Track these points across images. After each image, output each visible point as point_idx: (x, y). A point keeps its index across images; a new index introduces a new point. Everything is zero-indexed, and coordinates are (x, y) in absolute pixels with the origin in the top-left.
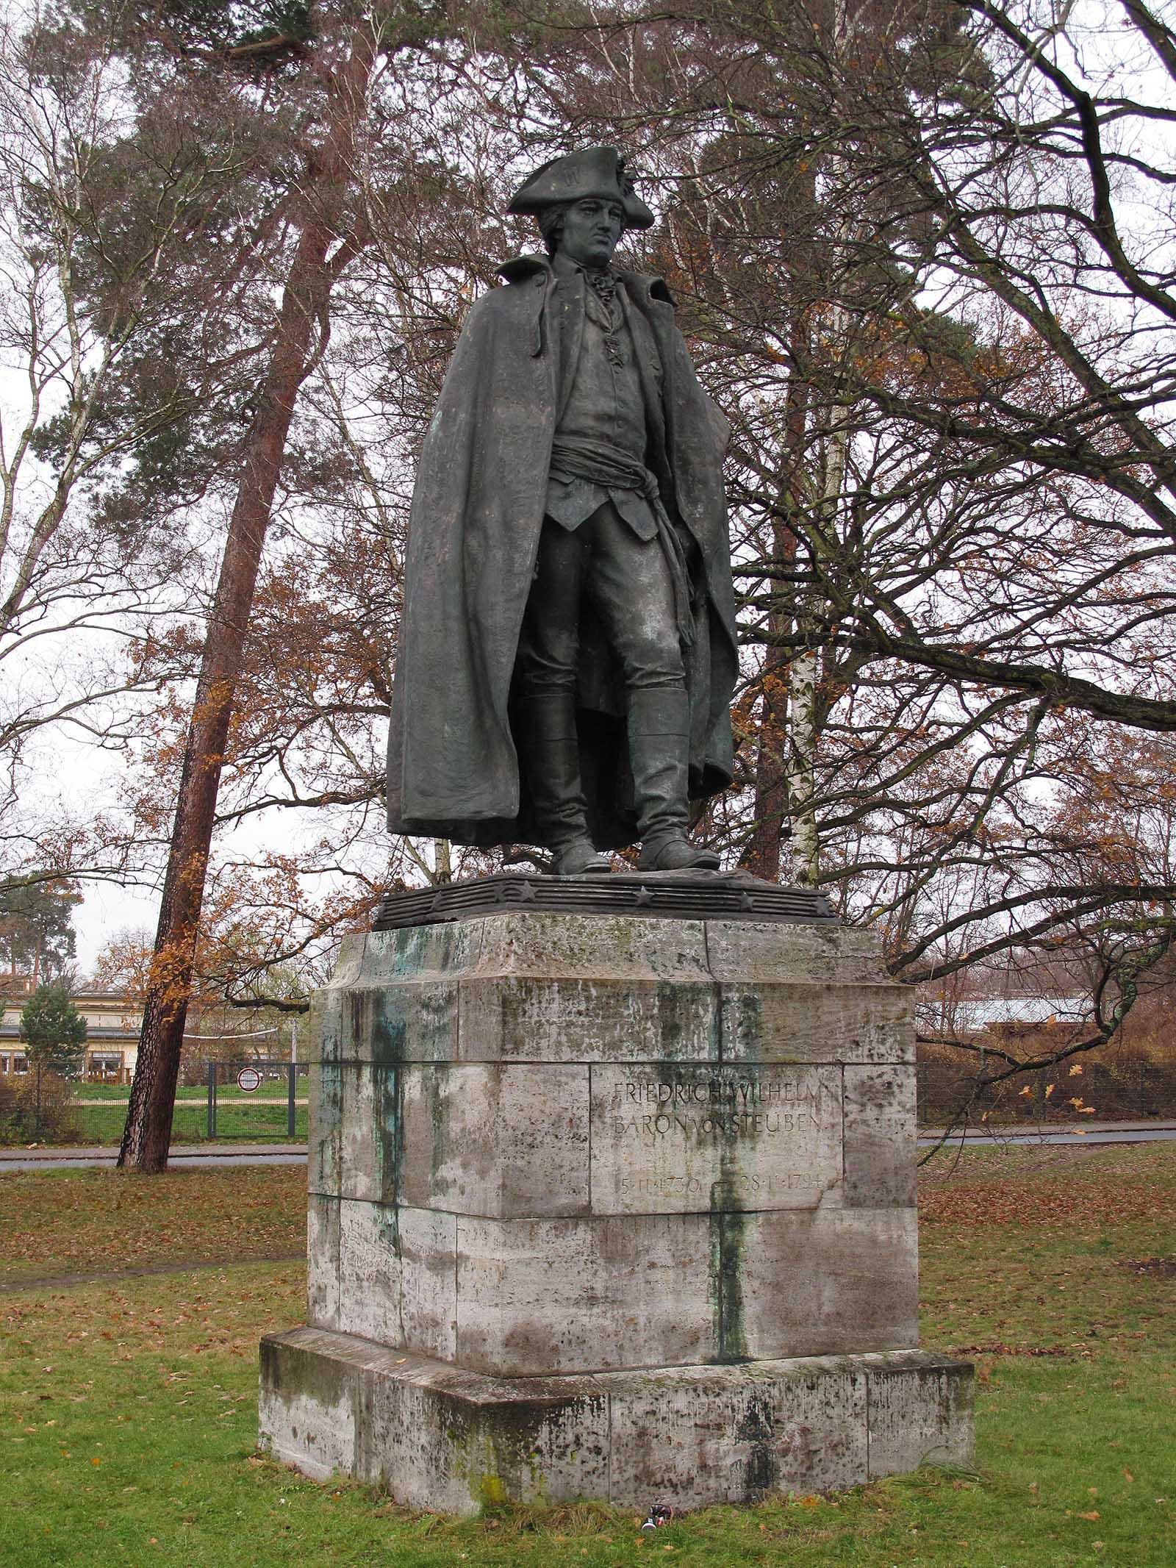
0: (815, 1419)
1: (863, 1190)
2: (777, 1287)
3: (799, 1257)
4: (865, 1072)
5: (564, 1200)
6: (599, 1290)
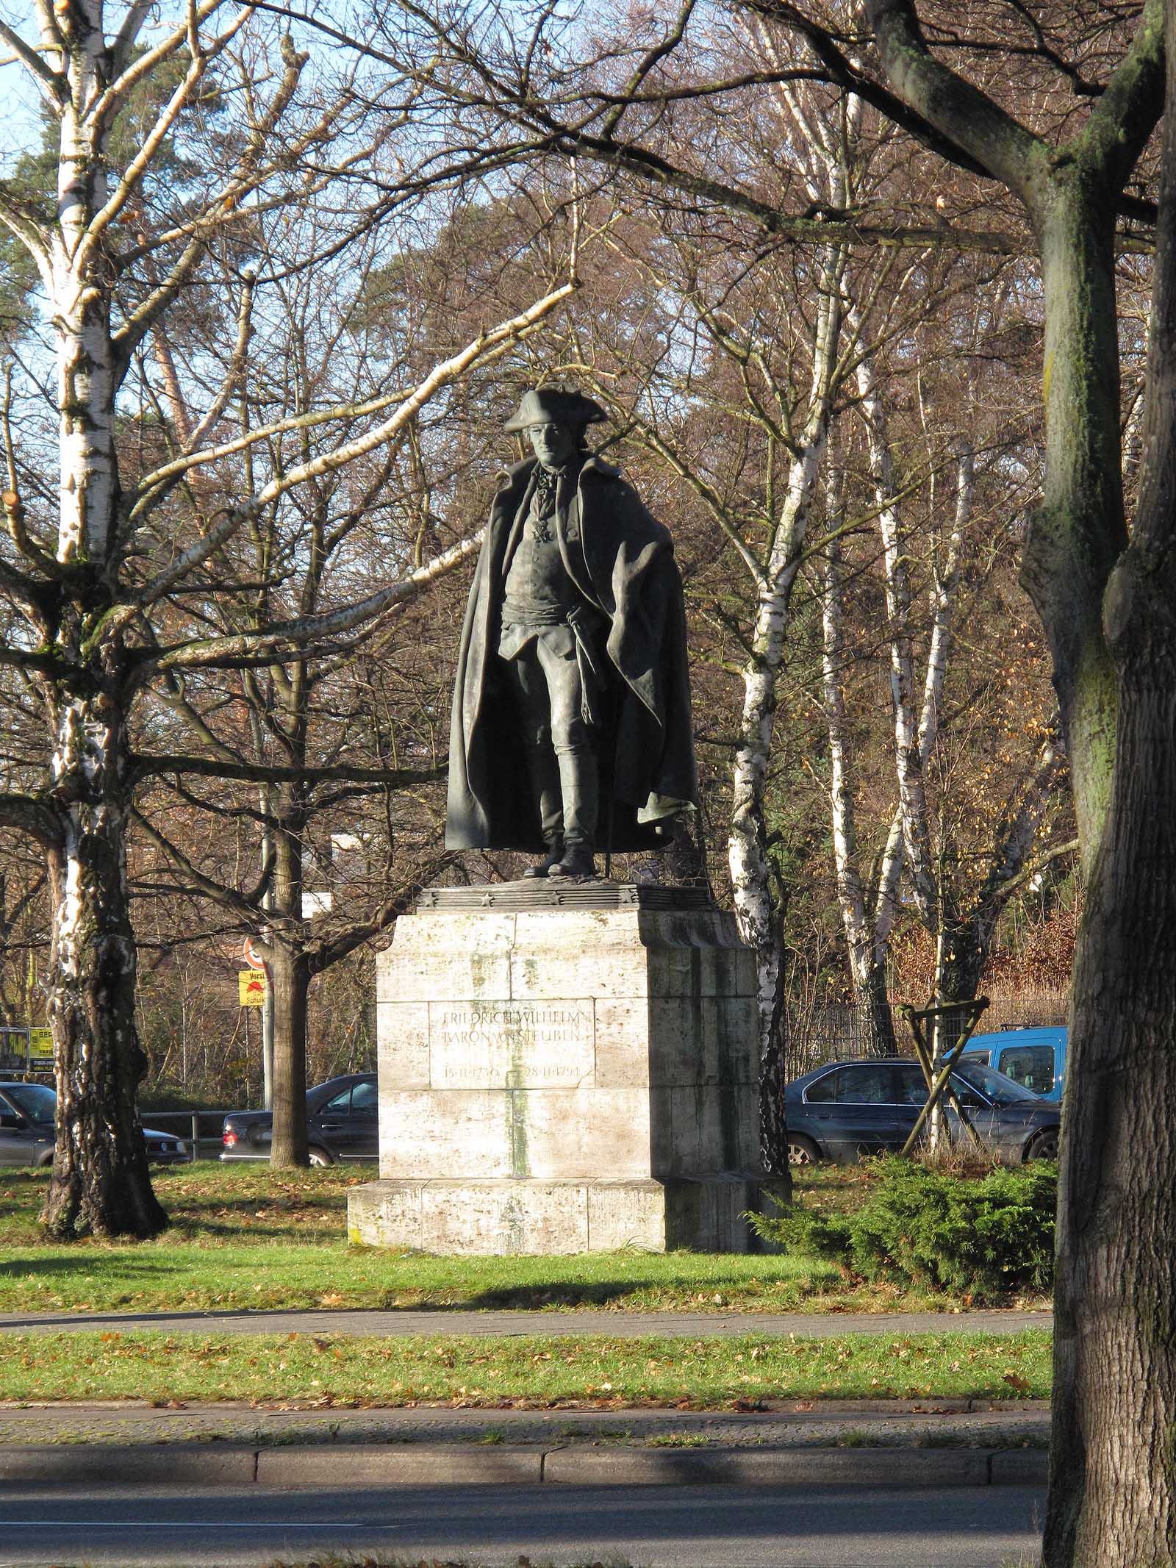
0: (552, 1213)
1: (609, 1077)
2: (551, 1134)
3: (564, 1118)
4: (609, 1004)
5: (415, 1080)
6: (437, 1133)
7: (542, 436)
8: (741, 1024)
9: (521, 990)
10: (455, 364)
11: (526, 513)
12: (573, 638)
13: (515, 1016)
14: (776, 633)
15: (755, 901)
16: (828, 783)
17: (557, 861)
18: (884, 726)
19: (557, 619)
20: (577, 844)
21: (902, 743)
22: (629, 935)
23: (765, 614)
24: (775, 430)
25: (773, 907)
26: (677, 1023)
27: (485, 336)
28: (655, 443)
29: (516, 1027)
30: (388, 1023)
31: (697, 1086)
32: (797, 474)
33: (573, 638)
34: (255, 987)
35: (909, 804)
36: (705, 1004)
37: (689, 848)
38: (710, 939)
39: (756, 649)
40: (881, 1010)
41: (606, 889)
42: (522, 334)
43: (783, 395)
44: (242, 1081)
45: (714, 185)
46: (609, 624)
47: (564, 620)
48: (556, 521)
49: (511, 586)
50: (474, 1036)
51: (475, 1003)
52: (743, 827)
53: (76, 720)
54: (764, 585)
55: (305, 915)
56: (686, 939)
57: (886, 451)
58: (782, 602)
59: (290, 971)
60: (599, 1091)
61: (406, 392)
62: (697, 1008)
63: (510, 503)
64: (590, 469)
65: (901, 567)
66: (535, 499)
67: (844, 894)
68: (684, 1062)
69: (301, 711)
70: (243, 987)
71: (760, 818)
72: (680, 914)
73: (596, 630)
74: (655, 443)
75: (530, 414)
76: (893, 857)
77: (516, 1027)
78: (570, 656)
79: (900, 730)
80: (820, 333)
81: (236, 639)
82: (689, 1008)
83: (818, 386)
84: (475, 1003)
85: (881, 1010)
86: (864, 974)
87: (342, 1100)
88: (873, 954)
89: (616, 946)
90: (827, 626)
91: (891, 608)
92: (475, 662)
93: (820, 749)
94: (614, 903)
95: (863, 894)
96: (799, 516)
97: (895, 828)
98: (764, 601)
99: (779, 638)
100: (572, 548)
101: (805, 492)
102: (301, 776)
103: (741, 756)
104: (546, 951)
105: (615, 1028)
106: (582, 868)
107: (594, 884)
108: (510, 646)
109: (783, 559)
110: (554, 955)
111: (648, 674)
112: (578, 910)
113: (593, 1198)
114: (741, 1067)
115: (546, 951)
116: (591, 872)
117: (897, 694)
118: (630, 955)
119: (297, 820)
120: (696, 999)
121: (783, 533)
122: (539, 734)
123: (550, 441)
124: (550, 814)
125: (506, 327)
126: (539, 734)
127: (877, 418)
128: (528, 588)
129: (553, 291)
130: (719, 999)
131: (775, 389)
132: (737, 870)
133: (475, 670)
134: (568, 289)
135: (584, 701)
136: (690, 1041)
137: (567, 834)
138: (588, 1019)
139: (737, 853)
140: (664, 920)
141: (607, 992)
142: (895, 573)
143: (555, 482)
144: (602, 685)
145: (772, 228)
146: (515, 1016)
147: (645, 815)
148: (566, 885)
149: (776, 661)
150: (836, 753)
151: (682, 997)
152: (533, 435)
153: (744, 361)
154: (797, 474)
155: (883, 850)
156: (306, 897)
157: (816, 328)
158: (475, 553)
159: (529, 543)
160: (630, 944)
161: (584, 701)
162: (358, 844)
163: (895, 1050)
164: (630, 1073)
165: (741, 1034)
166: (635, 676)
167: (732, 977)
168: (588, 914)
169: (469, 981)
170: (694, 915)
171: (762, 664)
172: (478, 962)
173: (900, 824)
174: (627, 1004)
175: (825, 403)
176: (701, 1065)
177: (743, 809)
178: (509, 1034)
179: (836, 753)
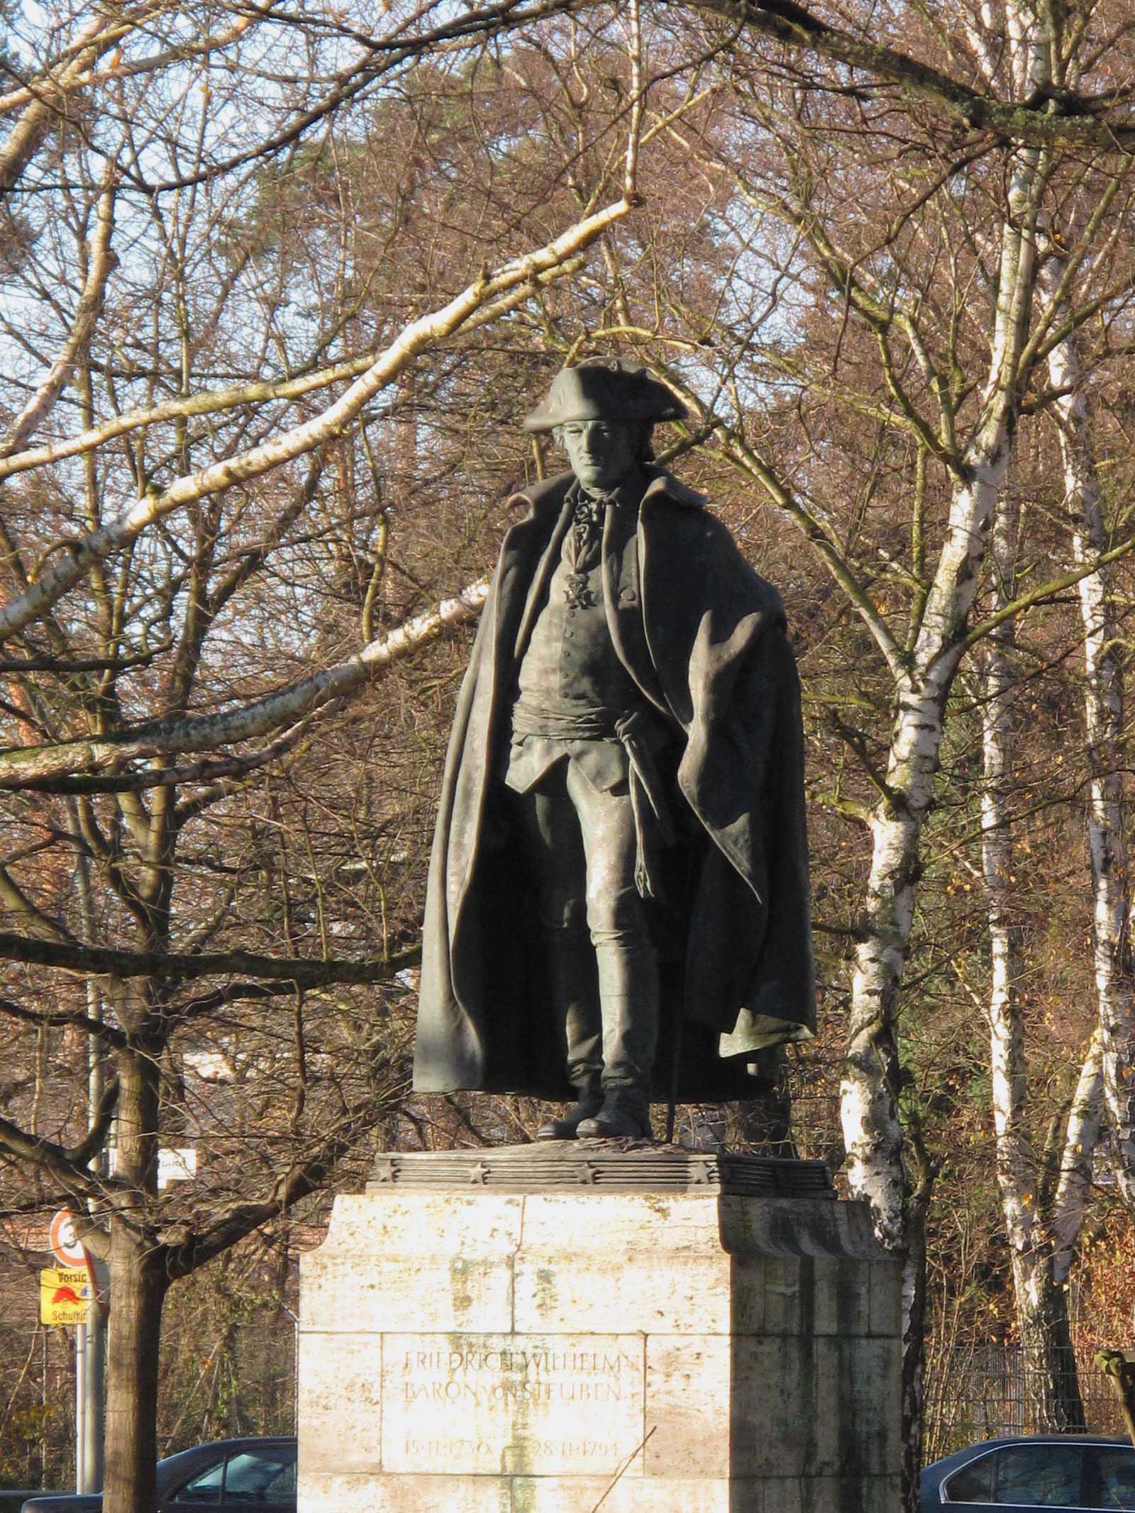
1: (666, 1460)
4: (669, 1343)
5: (356, 1457)
7: (583, 441)
8: (877, 1381)
9: (528, 1318)
10: (438, 322)
11: (555, 561)
12: (624, 760)
13: (518, 1359)
14: (924, 757)
15: (881, 1181)
16: (985, 993)
17: (590, 1114)
18: (1073, 905)
19: (601, 730)
20: (623, 1089)
21: (1102, 935)
22: (702, 1236)
23: (907, 726)
24: (931, 437)
25: (908, 1191)
26: (775, 1378)
27: (488, 278)
28: (739, 452)
29: (519, 1375)
30: (318, 1366)
31: (804, 1476)
32: (962, 506)
33: (624, 760)
34: (65, 1294)
35: (1113, 1031)
36: (820, 1347)
37: (756, 1092)
38: (830, 1243)
39: (892, 782)
40: (1060, 1356)
41: (669, 1160)
42: (543, 277)
43: (944, 382)
44: (33, 1442)
45: (887, 53)
46: (681, 741)
47: (612, 733)
48: (602, 575)
49: (529, 676)
50: (453, 1389)
51: (456, 1337)
52: (865, 1065)
54: (907, 682)
55: (162, 1184)
56: (793, 1243)
57: (1090, 472)
58: (934, 709)
59: (136, 1273)
60: (651, 1482)
61: (359, 363)
62: (807, 1354)
63: (529, 546)
64: (658, 495)
65: (1112, 656)
66: (569, 539)
67: (1005, 1172)
68: (786, 1439)
69: (165, 862)
70: (46, 1296)
71: (892, 1051)
72: (784, 1203)
73: (662, 749)
74: (739, 452)
75: (565, 403)
76: (1084, 1114)
77: (519, 1375)
78: (619, 789)
79: (1102, 912)
80: (1004, 286)
81: (78, 747)
82: (795, 1354)
83: (999, 367)
84: (456, 1337)
85: (1060, 1356)
86: (1035, 1299)
87: (211, 1479)
88: (1050, 1268)
89: (682, 1253)
90: (990, 749)
91: (1091, 720)
92: (468, 794)
93: (977, 942)
94: (680, 1183)
95: (1037, 1172)
96: (964, 573)
97: (1088, 1068)
98: (907, 707)
99: (928, 766)
100: (627, 619)
101: (973, 536)
102: (160, 967)
103: (864, 951)
104: (570, 1257)
105: (677, 1382)
106: (628, 1124)
107: (649, 1152)
108: (524, 771)
109: (937, 641)
110: (582, 1263)
111: (742, 821)
112: (621, 1192)
114: (874, 1448)
115: (570, 1257)
116: (643, 1133)
117: (1099, 858)
118: (703, 1267)
119: (154, 1034)
120: (806, 1339)
121: (939, 598)
122: (567, 913)
123: (596, 448)
124: (582, 1037)
125: (520, 265)
126: (567, 913)
127: (1078, 421)
128: (556, 680)
129: (594, 211)
130: (844, 1338)
131: (932, 372)
132: (854, 1134)
133: (467, 809)
134: (621, 207)
135: (640, 860)
136: (794, 1407)
137: (607, 1071)
138: (633, 1366)
139: (854, 1102)
140: (758, 1210)
141: (666, 1324)
142: (1099, 667)
143: (601, 513)
144: (669, 837)
145: (976, 124)
146: (518, 1359)
147: (732, 1044)
148: (606, 1153)
149: (922, 802)
150: (999, 947)
151: (784, 1336)
152: (568, 438)
153: (884, 327)
154: (962, 506)
155: (1070, 1103)
156: (164, 1156)
157: (997, 277)
158: (469, 620)
159: (558, 610)
160: (704, 1249)
161: (640, 860)
162: (226, 1072)
163: (1082, 1421)
164: (699, 1453)
165: (874, 1394)
166: (723, 821)
167: (863, 1306)
168: (639, 1201)
169: (445, 1304)
170: (807, 1205)
171: (900, 805)
172: (462, 1271)
173: (1098, 1060)
174: (697, 1344)
175: (1010, 397)
176: (809, 1447)
177: (865, 1034)
178: (508, 1387)
179: (999, 947)
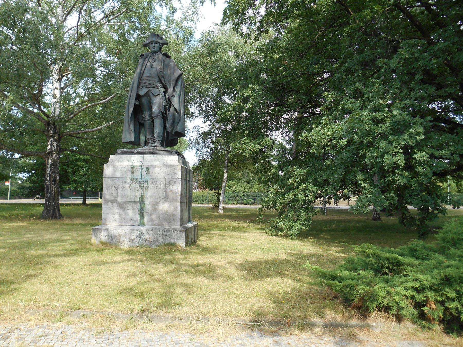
29: (143, 185)
53: (51, 141)
113: (164, 233)
146: (142, 182)
